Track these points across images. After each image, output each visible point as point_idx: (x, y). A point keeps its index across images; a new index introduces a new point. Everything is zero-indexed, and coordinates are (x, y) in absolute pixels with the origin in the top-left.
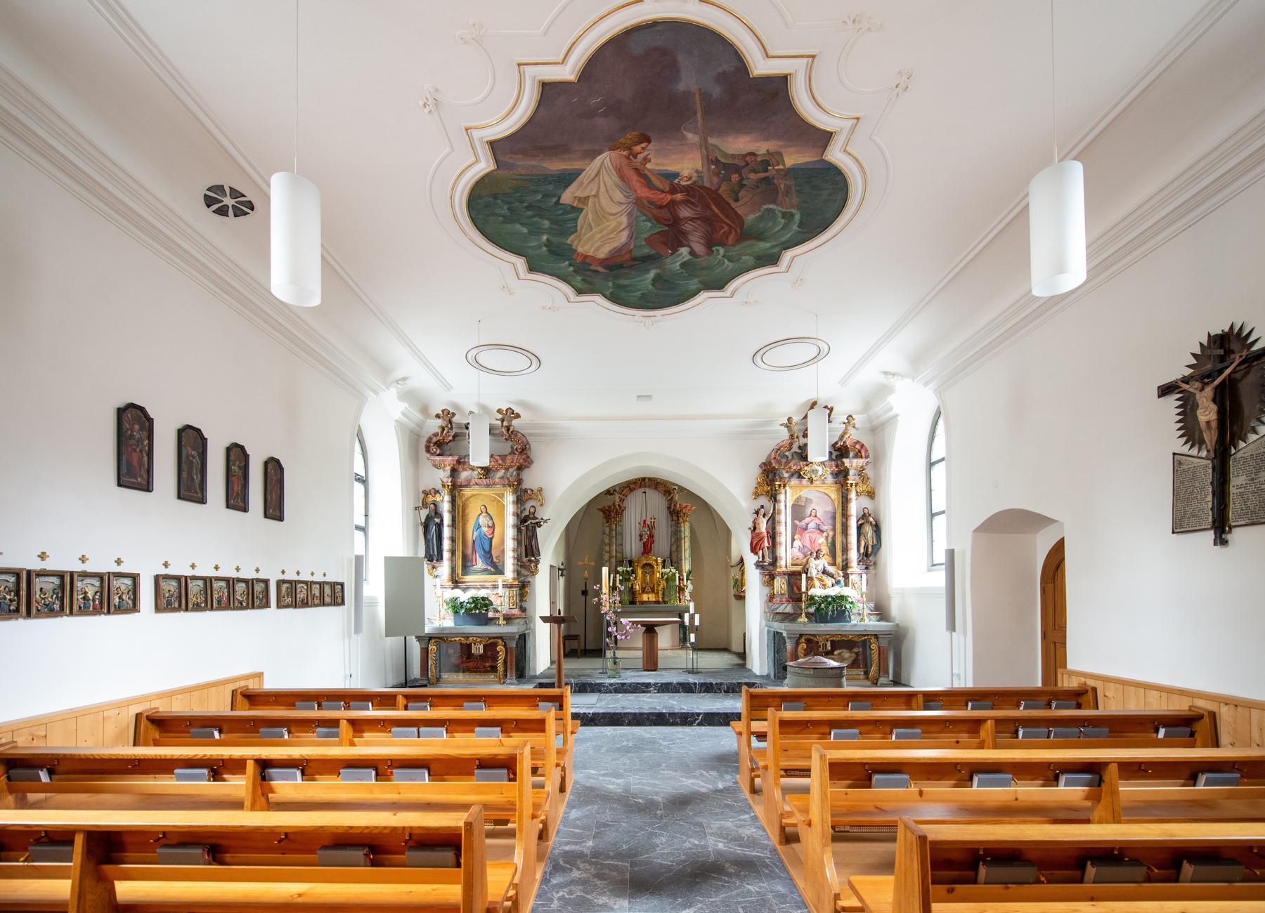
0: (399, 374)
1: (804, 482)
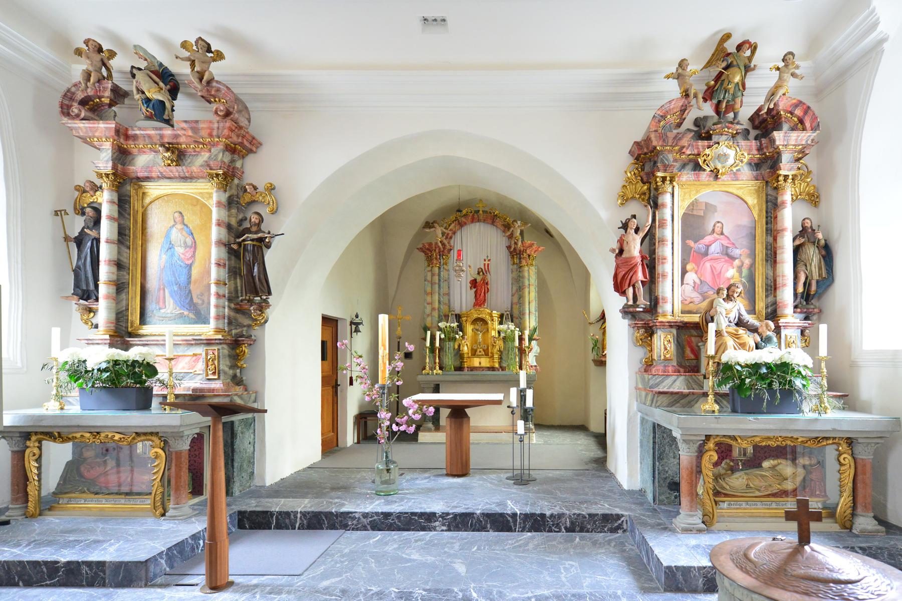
1: (704, 176)
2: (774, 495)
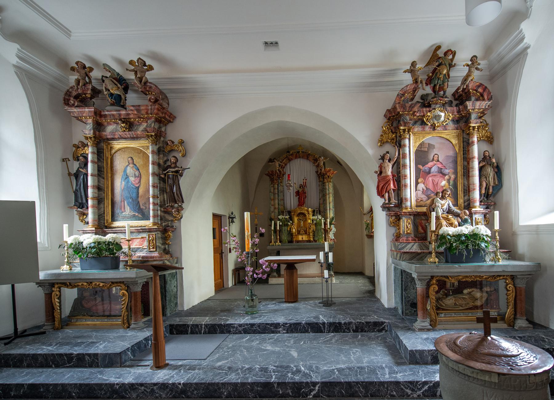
1: (427, 128)
2: (470, 309)
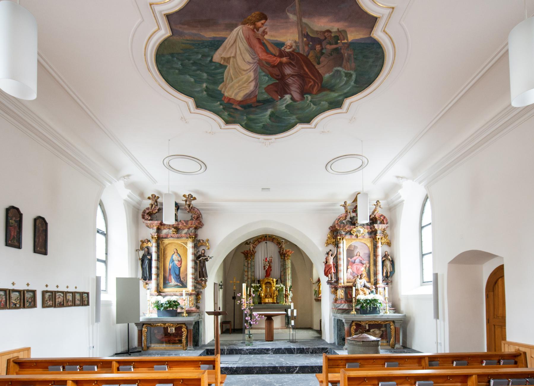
0: (125, 172)
1: (353, 237)
